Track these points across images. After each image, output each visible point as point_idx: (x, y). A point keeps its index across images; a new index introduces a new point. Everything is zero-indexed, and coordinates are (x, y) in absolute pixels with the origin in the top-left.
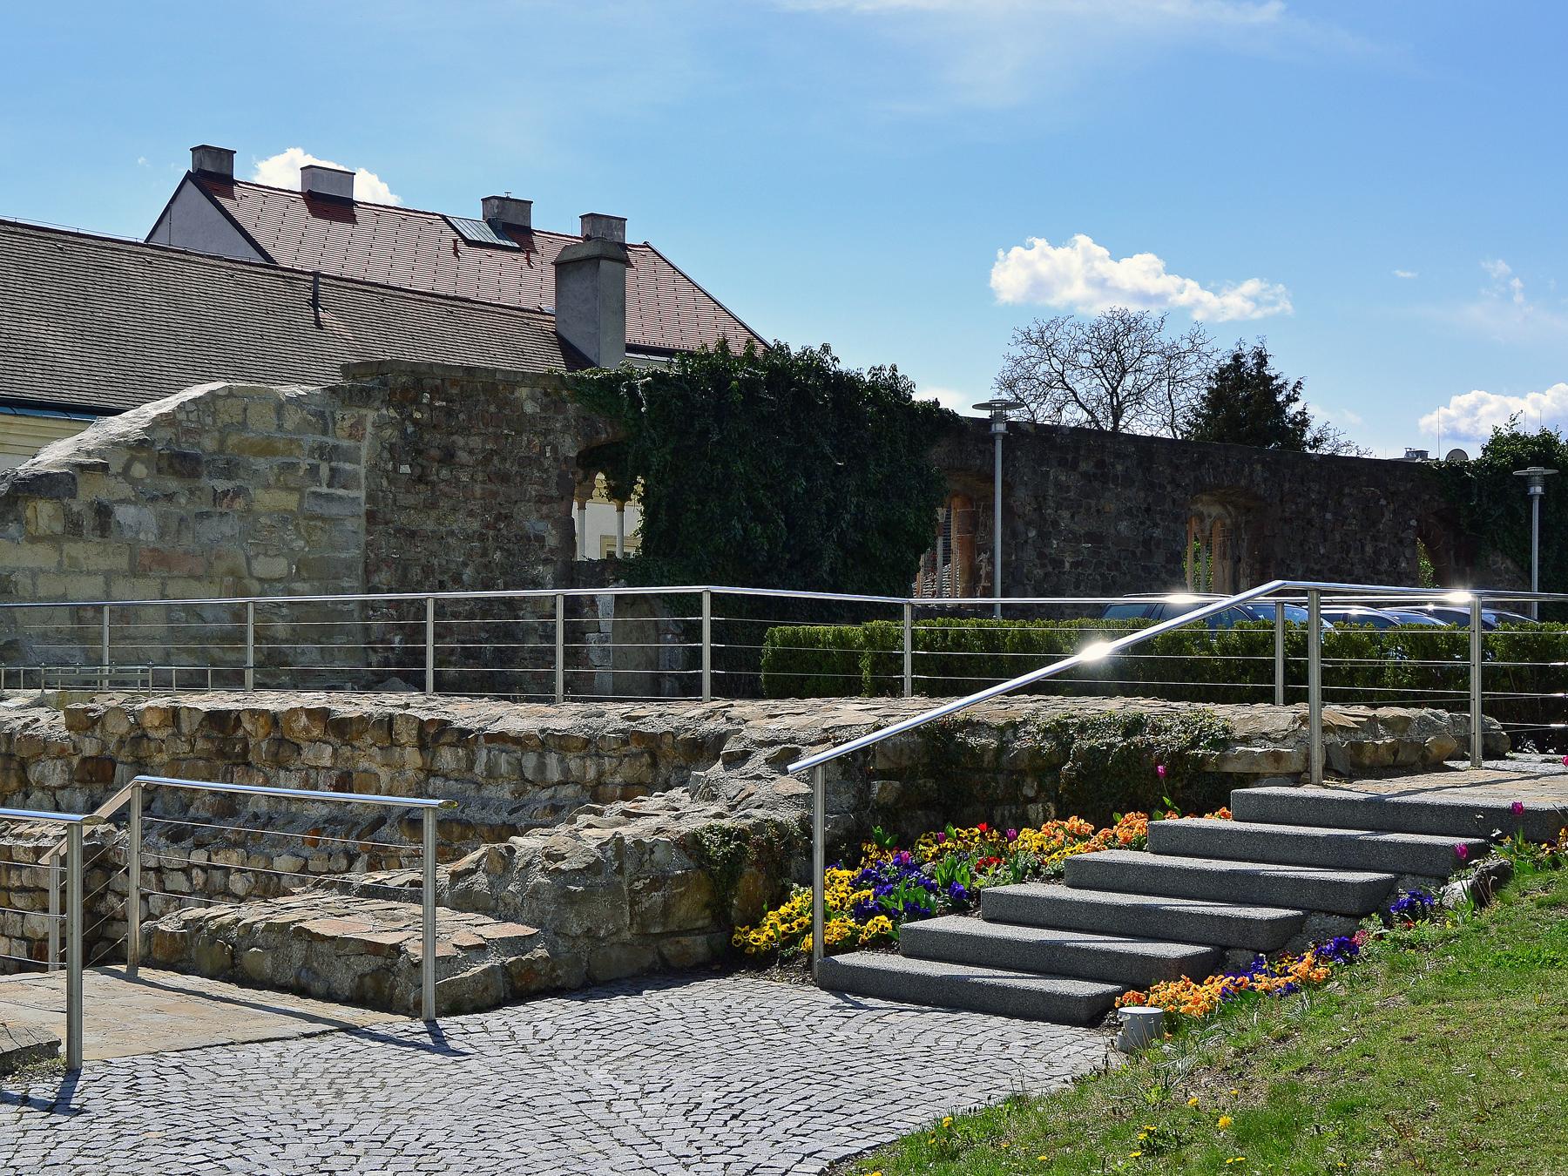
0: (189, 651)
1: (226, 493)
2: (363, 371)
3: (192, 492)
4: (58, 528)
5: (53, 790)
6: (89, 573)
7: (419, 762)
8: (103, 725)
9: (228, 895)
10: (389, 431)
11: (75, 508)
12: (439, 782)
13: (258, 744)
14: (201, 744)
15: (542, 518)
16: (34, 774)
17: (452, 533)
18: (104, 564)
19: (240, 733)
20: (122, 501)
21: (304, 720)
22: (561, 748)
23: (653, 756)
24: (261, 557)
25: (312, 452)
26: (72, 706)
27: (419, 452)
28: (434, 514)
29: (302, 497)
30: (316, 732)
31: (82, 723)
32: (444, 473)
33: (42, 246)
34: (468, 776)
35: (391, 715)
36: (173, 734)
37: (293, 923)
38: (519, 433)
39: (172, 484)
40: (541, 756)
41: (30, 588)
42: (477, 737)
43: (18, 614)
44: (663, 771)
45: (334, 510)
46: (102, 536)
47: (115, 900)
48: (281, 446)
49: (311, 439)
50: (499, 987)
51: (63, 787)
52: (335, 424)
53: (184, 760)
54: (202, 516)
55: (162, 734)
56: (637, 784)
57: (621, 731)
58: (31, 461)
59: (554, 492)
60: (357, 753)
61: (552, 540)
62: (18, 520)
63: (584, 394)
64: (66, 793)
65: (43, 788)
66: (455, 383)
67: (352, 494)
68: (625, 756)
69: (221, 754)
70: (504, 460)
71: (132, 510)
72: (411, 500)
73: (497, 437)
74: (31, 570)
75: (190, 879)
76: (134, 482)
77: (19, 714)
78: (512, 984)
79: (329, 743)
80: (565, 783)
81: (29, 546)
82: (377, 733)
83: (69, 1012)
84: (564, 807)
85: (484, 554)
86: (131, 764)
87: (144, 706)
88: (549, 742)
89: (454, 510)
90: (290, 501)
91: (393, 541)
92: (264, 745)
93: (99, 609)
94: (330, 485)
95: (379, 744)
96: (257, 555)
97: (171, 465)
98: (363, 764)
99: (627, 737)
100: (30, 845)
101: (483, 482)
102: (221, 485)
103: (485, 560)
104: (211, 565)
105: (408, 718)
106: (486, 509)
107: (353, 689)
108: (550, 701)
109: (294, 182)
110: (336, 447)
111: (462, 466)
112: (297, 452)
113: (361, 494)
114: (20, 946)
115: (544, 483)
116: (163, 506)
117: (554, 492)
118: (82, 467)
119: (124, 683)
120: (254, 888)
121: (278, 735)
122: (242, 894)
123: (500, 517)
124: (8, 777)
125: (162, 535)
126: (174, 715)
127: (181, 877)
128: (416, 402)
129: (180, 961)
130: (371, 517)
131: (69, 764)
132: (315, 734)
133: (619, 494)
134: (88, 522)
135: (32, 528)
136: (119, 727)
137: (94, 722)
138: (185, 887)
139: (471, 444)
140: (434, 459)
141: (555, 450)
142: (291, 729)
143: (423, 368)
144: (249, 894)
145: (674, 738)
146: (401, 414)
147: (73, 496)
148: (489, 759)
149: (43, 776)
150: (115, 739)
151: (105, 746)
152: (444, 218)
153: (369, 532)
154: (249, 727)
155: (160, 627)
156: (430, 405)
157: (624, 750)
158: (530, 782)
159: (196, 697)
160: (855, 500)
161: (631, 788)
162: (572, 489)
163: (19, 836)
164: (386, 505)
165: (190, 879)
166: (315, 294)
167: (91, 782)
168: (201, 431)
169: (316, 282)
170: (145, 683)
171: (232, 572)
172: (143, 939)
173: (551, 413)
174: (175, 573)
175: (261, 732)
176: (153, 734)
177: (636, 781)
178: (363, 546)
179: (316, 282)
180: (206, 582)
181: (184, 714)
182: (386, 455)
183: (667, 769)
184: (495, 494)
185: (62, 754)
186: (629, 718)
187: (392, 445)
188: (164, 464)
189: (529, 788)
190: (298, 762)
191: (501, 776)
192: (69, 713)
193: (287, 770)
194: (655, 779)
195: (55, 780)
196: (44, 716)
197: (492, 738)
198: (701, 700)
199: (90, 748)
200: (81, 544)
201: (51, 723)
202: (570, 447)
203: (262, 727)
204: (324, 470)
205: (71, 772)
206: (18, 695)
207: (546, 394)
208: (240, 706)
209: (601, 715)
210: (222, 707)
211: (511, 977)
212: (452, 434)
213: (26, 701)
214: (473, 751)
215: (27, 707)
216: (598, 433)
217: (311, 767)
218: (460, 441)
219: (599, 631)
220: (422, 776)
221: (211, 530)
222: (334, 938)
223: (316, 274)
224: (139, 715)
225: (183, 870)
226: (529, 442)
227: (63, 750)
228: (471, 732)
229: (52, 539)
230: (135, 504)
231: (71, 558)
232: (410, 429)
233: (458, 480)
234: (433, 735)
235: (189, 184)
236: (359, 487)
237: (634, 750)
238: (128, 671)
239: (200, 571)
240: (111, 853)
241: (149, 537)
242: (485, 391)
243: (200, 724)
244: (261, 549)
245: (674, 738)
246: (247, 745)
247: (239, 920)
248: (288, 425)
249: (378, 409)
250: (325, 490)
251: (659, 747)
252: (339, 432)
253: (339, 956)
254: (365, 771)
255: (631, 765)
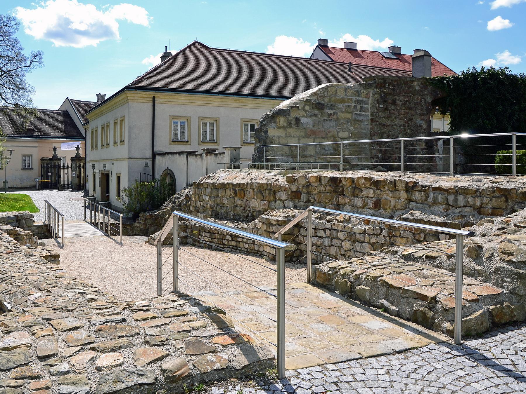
0: (322, 159)
1: (331, 114)
2: (369, 79)
3: (322, 114)
4: (285, 124)
5: (283, 201)
6: (294, 137)
7: (406, 197)
8: (298, 181)
9: (338, 239)
10: (377, 96)
11: (290, 119)
12: (414, 204)
13: (347, 188)
14: (328, 188)
15: (421, 120)
16: (277, 196)
17: (395, 125)
18: (298, 134)
19: (341, 185)
20: (303, 116)
21: (363, 181)
22: (465, 193)
23: (506, 197)
24: (341, 132)
25: (355, 102)
26: (288, 175)
27: (386, 101)
28: (390, 119)
29: (352, 115)
30: (367, 185)
31: (292, 181)
32: (393, 107)
33: (283, 60)
34: (426, 202)
35: (395, 180)
36: (319, 185)
37: (379, 277)
38: (414, 95)
39: (316, 112)
40: (456, 196)
41: (278, 141)
42: (429, 188)
43: (275, 149)
44: (510, 203)
45: (361, 118)
46: (297, 126)
47: (301, 237)
48: (346, 100)
49: (355, 98)
50: (487, 324)
51: (286, 200)
52: (361, 94)
53: (323, 193)
54: (325, 120)
55: (316, 184)
56: (498, 208)
57: (492, 187)
58: (278, 106)
59: (425, 112)
60: (382, 192)
61: (424, 126)
62: (275, 122)
63: (433, 83)
64: (287, 202)
65: (280, 200)
66: (395, 81)
67: (367, 114)
68: (493, 197)
69: (335, 191)
70: (410, 103)
71: (305, 119)
72: (383, 115)
73: (408, 97)
74: (278, 136)
75: (325, 233)
76: (306, 111)
77: (274, 177)
78: (493, 319)
79: (372, 189)
80: (466, 207)
81: (278, 130)
82: (390, 186)
83: (278, 322)
84: (466, 216)
85: (405, 130)
86: (306, 193)
87: (310, 175)
88: (458, 191)
89: (396, 118)
90: (349, 116)
91: (378, 127)
92: (349, 189)
93: (296, 146)
94: (360, 111)
95: (390, 190)
96: (340, 131)
97: (316, 106)
98: (385, 196)
99: (493, 191)
100: (276, 219)
101: (404, 110)
102: (330, 111)
103: (405, 132)
104: (327, 134)
105: (401, 181)
106: (405, 118)
107: (367, 170)
108: (449, 175)
109: (342, 46)
110: (362, 101)
111: (398, 105)
112: (351, 102)
113: (369, 114)
114: (273, 250)
115: (422, 110)
116: (314, 118)
117: (425, 112)
118: (292, 107)
119: (303, 168)
120: (347, 237)
121: (354, 186)
122: (343, 239)
123: (409, 120)
124: (270, 196)
125: (314, 126)
126: (320, 178)
127: (322, 232)
128: (384, 87)
129: (328, 284)
130: (372, 120)
131: (288, 193)
132: (367, 186)
133: (443, 113)
134: (293, 123)
135: (278, 124)
136: (303, 182)
137: (295, 180)
138: (324, 235)
139: (401, 99)
140: (390, 103)
141: (425, 100)
142: (359, 184)
143: (386, 77)
144: (345, 239)
145: (517, 191)
146: (380, 90)
147: (289, 115)
148: (434, 196)
149: (280, 196)
150: (301, 186)
151: (298, 188)
152: (379, 52)
153: (371, 125)
154: (344, 183)
155: (313, 152)
156: (388, 88)
157: (492, 195)
158: (451, 205)
159: (326, 173)
160: (517, 113)
161: (496, 210)
162: (430, 112)
163: (273, 216)
164: (376, 117)
165: (325, 233)
166: (350, 68)
167: (294, 199)
168: (324, 97)
169: (350, 66)
170: (310, 168)
171: (333, 136)
172: (313, 273)
173: (423, 89)
174: (317, 137)
175: (348, 185)
176: (312, 184)
177: (498, 207)
178: (370, 129)
179: (350, 66)
180: (326, 139)
181: (322, 178)
182: (376, 102)
183: (512, 203)
184: (407, 113)
185: (285, 190)
186: (494, 182)
187: (377, 99)
188: (314, 106)
189: (451, 208)
190: (361, 195)
191: (439, 203)
192: (287, 177)
193: (357, 197)
194: (507, 207)
195: (284, 198)
196: (280, 178)
197: (435, 189)
198: (512, 175)
199: (294, 188)
200: (292, 129)
201: (282, 181)
202: (429, 99)
203: (349, 183)
204: (359, 107)
205: (288, 195)
206: (273, 171)
207: (422, 84)
208: (341, 176)
209: (481, 181)
210: (335, 176)
211: (492, 316)
212: (395, 96)
213: (275, 173)
214: (427, 193)
215: (276, 175)
216: (437, 95)
217: (366, 197)
218: (397, 98)
219: (439, 153)
220: (407, 202)
221: (327, 124)
222: (400, 288)
223: (350, 63)
224: (309, 178)
225: (323, 230)
226: (417, 98)
227: (286, 189)
228: (426, 186)
229: (284, 128)
230: (306, 117)
231: (289, 133)
232: (383, 95)
233: (397, 109)
234: (411, 188)
235: (317, 48)
236: (368, 112)
237: (497, 195)
238: (304, 164)
239: (324, 136)
240: (300, 222)
241: (310, 127)
242: (404, 83)
243: (328, 182)
244: (341, 130)
245: (517, 191)
246: (343, 189)
247: (354, 271)
248: (349, 94)
249: (373, 89)
250: (359, 113)
251: (509, 194)
252: (362, 96)
253: (403, 297)
254: (385, 199)
255: (496, 201)
